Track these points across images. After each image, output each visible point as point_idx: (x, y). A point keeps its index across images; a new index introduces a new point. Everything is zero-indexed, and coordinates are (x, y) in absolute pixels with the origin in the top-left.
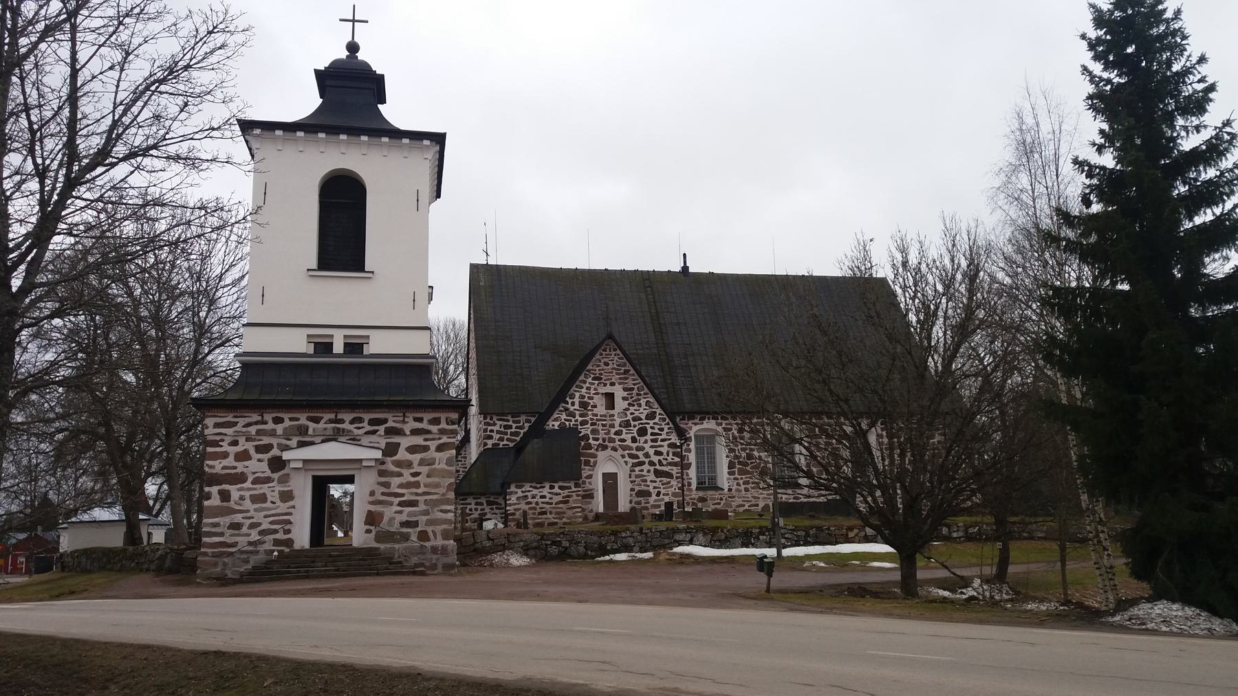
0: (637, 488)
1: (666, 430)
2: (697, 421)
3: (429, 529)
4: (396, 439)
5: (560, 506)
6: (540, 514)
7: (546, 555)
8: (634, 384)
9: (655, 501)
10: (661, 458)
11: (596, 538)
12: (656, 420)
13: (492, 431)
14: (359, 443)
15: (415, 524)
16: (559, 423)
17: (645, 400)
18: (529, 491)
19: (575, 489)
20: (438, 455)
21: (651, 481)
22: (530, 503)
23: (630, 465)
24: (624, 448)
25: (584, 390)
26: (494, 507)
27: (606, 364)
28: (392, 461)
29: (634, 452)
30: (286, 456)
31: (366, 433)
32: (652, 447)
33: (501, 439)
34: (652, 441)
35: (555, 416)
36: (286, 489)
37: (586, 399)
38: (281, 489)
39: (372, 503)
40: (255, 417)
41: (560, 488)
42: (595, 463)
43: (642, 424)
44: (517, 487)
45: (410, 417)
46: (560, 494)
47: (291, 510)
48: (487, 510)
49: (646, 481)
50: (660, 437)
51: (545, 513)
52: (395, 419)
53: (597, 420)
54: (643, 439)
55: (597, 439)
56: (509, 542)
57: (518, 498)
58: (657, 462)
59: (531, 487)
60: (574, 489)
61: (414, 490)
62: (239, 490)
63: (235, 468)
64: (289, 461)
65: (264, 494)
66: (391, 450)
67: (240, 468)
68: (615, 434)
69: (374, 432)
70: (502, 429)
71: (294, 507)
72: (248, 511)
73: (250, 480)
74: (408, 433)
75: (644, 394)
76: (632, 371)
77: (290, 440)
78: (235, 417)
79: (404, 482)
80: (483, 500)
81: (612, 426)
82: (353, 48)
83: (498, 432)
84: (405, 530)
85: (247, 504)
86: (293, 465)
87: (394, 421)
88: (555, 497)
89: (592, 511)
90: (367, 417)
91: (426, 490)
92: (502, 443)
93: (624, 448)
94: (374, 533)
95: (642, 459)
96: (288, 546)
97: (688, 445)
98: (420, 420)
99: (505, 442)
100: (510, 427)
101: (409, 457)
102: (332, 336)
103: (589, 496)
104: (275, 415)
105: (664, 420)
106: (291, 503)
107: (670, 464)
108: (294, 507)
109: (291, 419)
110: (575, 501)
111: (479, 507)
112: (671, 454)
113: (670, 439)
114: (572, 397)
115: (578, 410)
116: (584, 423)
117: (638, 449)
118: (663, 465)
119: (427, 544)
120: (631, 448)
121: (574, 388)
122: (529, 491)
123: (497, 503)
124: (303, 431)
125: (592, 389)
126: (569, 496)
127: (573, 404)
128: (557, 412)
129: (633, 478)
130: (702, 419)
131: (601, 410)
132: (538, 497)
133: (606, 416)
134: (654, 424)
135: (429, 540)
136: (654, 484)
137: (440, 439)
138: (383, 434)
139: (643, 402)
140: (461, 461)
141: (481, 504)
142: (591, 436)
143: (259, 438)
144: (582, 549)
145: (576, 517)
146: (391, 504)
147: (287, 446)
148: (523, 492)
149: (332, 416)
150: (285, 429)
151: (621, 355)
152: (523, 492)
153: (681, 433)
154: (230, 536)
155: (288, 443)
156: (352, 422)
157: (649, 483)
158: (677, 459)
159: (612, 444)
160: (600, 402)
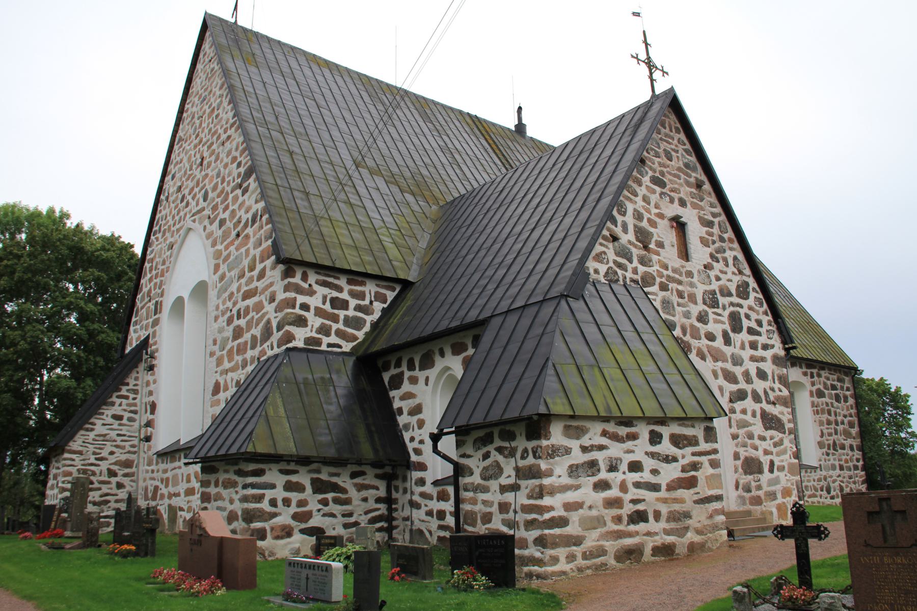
13: (305, 307)
18: (601, 448)
26: (330, 496)
33: (324, 330)
46: (675, 459)
48: (313, 505)
57: (573, 470)
59: (604, 434)
80: (304, 478)
88: (663, 467)
92: (326, 340)
99: (333, 339)
100: (344, 305)
111: (295, 496)
122: (601, 448)
123: (335, 488)
131: (670, 254)
132: (624, 467)
141: (299, 488)
152: (584, 449)
160: (664, 233)
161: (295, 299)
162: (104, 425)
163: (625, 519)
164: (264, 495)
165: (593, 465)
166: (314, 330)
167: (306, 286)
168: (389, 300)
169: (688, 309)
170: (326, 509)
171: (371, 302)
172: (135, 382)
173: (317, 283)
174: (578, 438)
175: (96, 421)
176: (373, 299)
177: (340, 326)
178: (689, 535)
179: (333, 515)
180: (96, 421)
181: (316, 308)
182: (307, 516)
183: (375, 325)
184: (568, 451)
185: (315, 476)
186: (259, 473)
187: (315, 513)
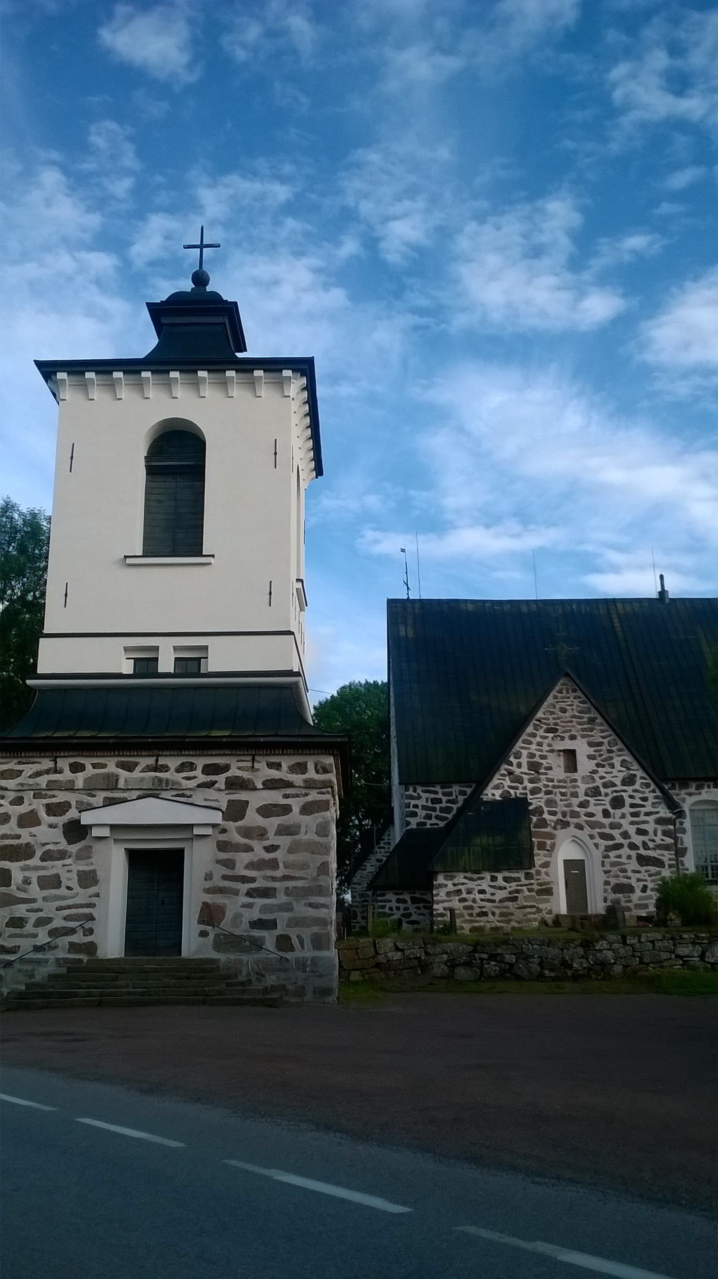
0: (613, 881)
1: (651, 800)
2: (692, 790)
3: (293, 934)
4: (242, 796)
5: (506, 904)
6: (479, 915)
7: (482, 974)
8: (604, 738)
9: (641, 899)
10: (645, 838)
11: (556, 951)
12: (637, 786)
13: (416, 806)
14: (190, 800)
15: (272, 925)
16: (500, 791)
17: (620, 759)
18: (463, 884)
19: (526, 882)
20: (306, 819)
21: (634, 871)
22: (464, 900)
23: (602, 848)
24: (593, 825)
25: (534, 747)
26: (421, 905)
27: (564, 710)
28: (237, 828)
29: (607, 830)
30: (87, 818)
31: (199, 786)
32: (632, 823)
33: (428, 817)
34: (634, 815)
35: (495, 781)
36: (86, 868)
37: (537, 759)
38: (81, 868)
39: (208, 891)
40: (47, 764)
41: (506, 879)
42: (553, 846)
43: (616, 791)
44: (446, 878)
45: (261, 764)
46: (505, 888)
47: (94, 900)
48: (412, 910)
49: (625, 871)
50: (643, 810)
51: (484, 914)
52: (241, 764)
53: (554, 787)
54: (618, 812)
55: (553, 813)
56: (427, 953)
57: (448, 894)
58: (640, 844)
59: (465, 878)
60: (524, 881)
61: (269, 873)
62: (25, 869)
63: (18, 837)
64: (90, 827)
65: (57, 876)
66: (236, 811)
67: (25, 835)
68: (579, 806)
69: (210, 785)
70: (430, 804)
71: (97, 895)
72: (34, 901)
73: (39, 853)
74: (260, 786)
75: (619, 750)
76: (599, 720)
77: (94, 796)
78: (19, 763)
79: (255, 860)
81: (575, 795)
82: (200, 279)
83: (424, 808)
84: (256, 933)
85: (34, 890)
86: (95, 832)
87: (239, 768)
89: (550, 912)
90: (200, 762)
91: (287, 872)
92: (429, 822)
93: (593, 825)
94: (211, 936)
95: (619, 840)
96: (89, 954)
97: (682, 823)
98: (278, 766)
99: (434, 821)
100: (439, 801)
101: (260, 821)
102: (156, 649)
103: (547, 891)
104: (72, 760)
105: (648, 786)
106: (93, 890)
107: (659, 847)
108: (97, 895)
109: (94, 766)
110: (526, 898)
111: (402, 906)
112: (659, 833)
113: (658, 813)
114: (518, 756)
115: (526, 774)
116: (534, 791)
117: (613, 826)
118: (649, 849)
119: (289, 955)
120: (602, 826)
121: (520, 743)
122: (463, 884)
124: (111, 783)
125: (544, 745)
126: (517, 891)
127: (519, 765)
128: (497, 776)
129: (608, 867)
130: (700, 787)
131: (558, 772)
133: (565, 782)
134: (635, 791)
135: (292, 949)
136: (638, 876)
137: (306, 795)
138: (223, 787)
139: (617, 761)
140: (384, 848)
141: (405, 901)
142: (545, 809)
143: (51, 793)
144: (535, 968)
145: (530, 920)
146: (236, 893)
147: (89, 804)
148: (454, 885)
149: (151, 761)
150: (86, 780)
151: (584, 698)
152: (454, 885)
153: (672, 805)
154: (10, 936)
155: (91, 800)
156: (178, 771)
157: (630, 874)
158: (669, 841)
159: (575, 820)
161: (410, 803)
162: (371, 866)
163: (475, 914)
164: (386, 905)
165: (459, 892)
166: (422, 817)
167: (416, 794)
168: (468, 793)
169: (569, 801)
170: (419, 912)
171: (457, 796)
172: (388, 838)
173: (423, 791)
174: (451, 880)
175: (367, 864)
176: (457, 794)
177: (438, 813)
178: (512, 923)
179: (423, 914)
180: (367, 864)
181: (423, 806)
182: (410, 915)
183: (458, 809)
184: (446, 886)
185: (412, 895)
186: (383, 895)
187: (413, 914)
